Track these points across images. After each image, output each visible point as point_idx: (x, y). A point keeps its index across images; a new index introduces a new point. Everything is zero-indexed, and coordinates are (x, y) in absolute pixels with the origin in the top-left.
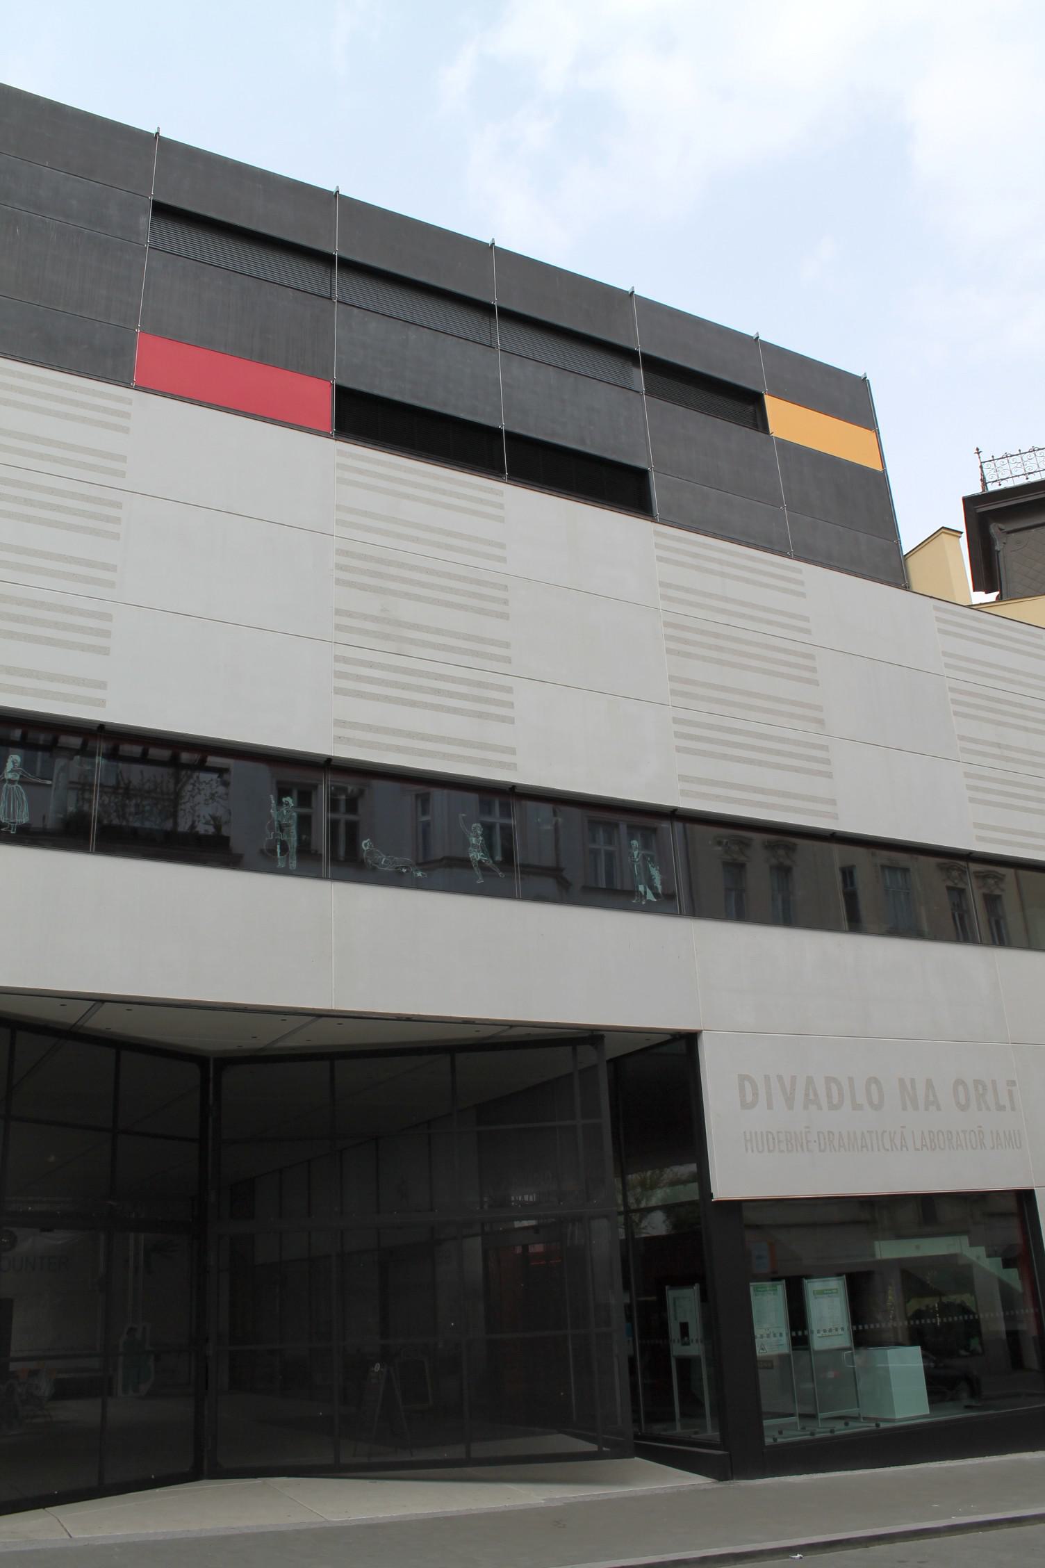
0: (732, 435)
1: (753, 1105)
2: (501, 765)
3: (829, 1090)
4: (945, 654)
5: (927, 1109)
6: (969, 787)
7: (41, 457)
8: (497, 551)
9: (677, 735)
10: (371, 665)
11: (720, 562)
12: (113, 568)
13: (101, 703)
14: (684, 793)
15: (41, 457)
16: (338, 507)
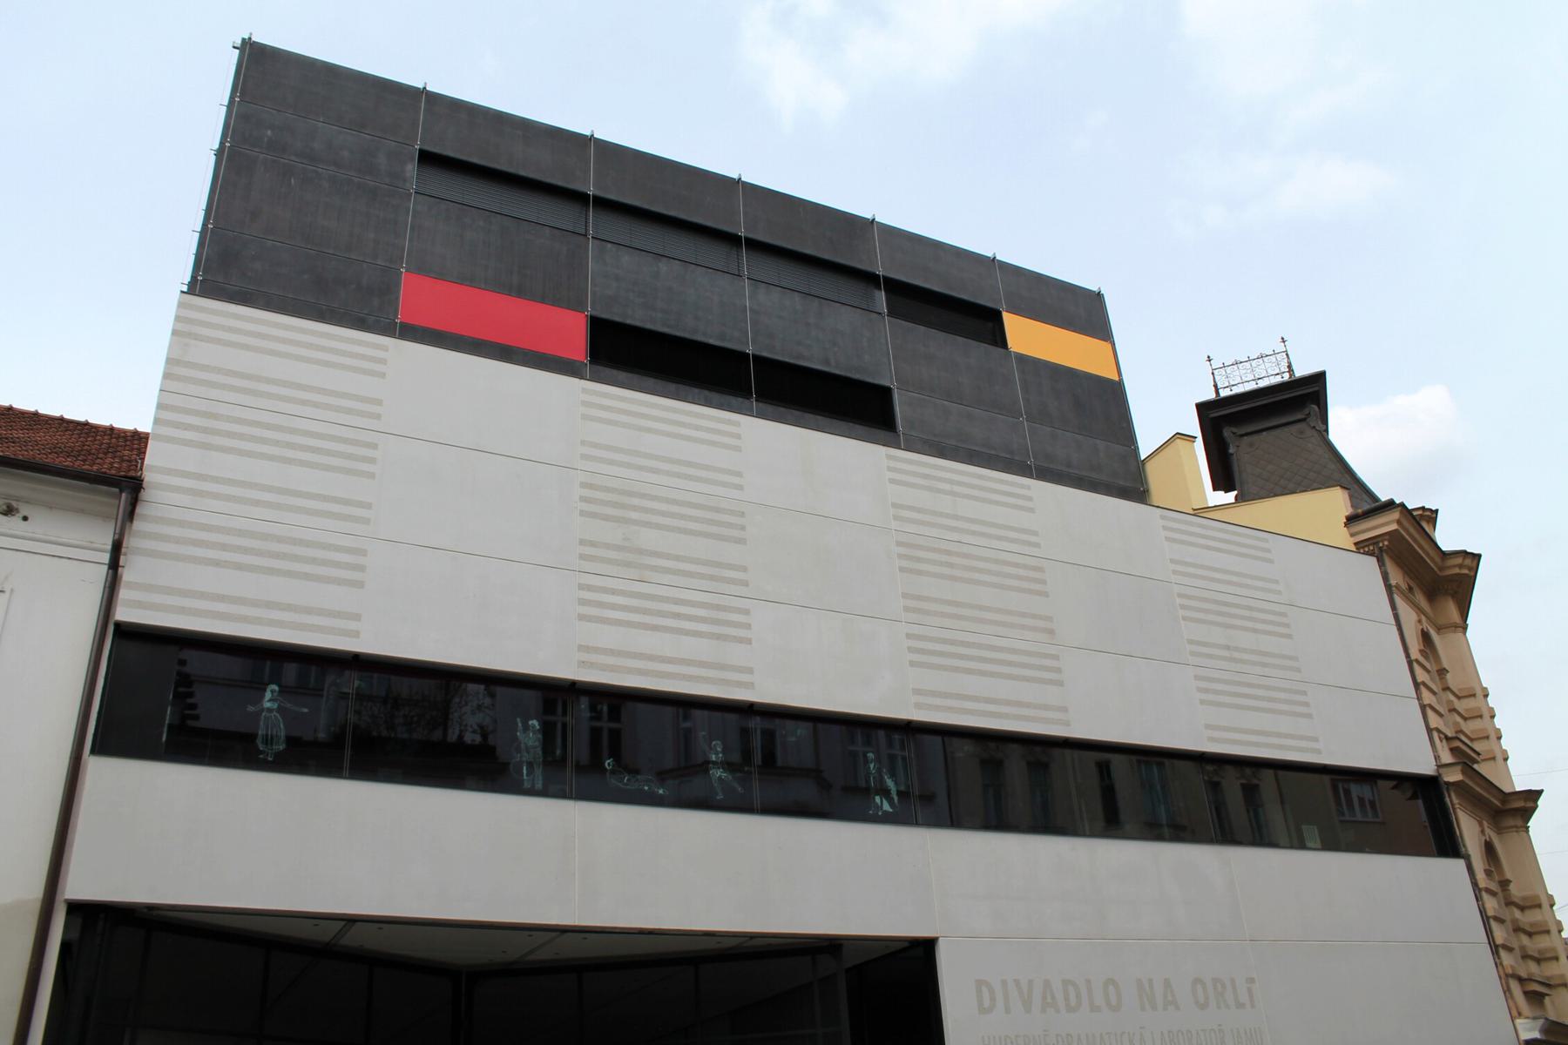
0: (972, 353)
1: (990, 1010)
2: (740, 684)
4: (1172, 561)
5: (1165, 1009)
6: (1200, 690)
7: (304, 402)
8: (736, 480)
9: (910, 649)
10: (613, 592)
11: (951, 482)
12: (369, 506)
13: (356, 634)
14: (918, 706)
15: (304, 402)
16: (583, 443)
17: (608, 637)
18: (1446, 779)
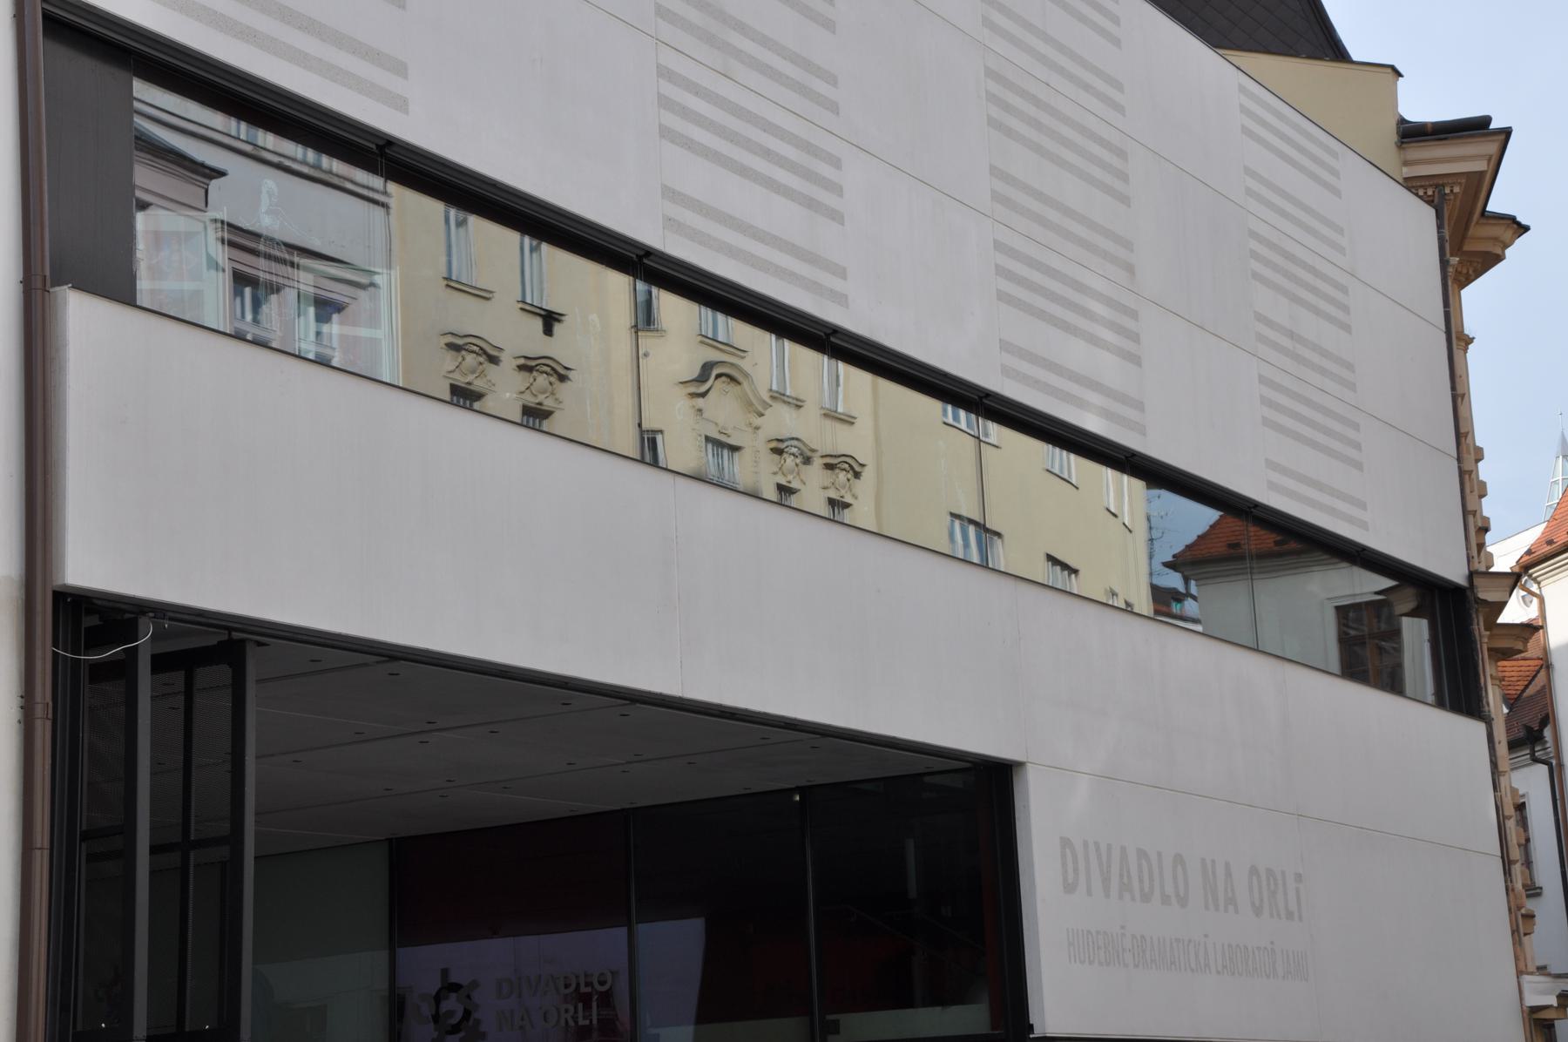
3: (1140, 866)
14: (1007, 371)
17: (697, 178)
18: (1482, 595)
